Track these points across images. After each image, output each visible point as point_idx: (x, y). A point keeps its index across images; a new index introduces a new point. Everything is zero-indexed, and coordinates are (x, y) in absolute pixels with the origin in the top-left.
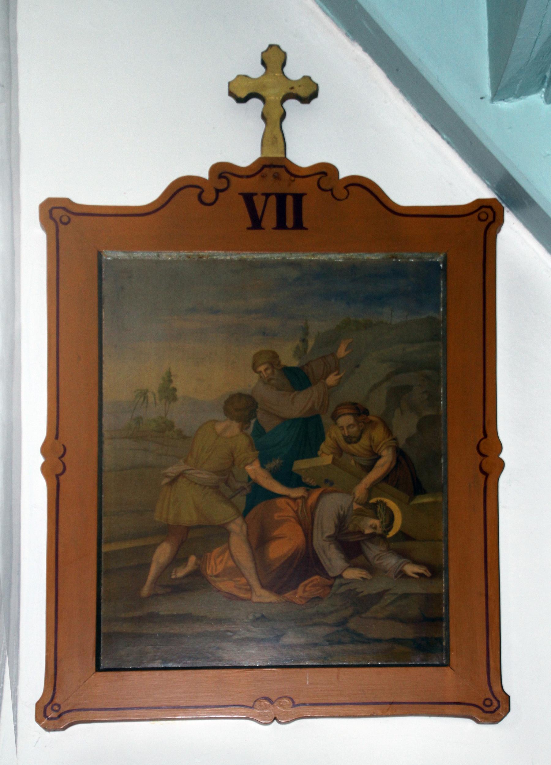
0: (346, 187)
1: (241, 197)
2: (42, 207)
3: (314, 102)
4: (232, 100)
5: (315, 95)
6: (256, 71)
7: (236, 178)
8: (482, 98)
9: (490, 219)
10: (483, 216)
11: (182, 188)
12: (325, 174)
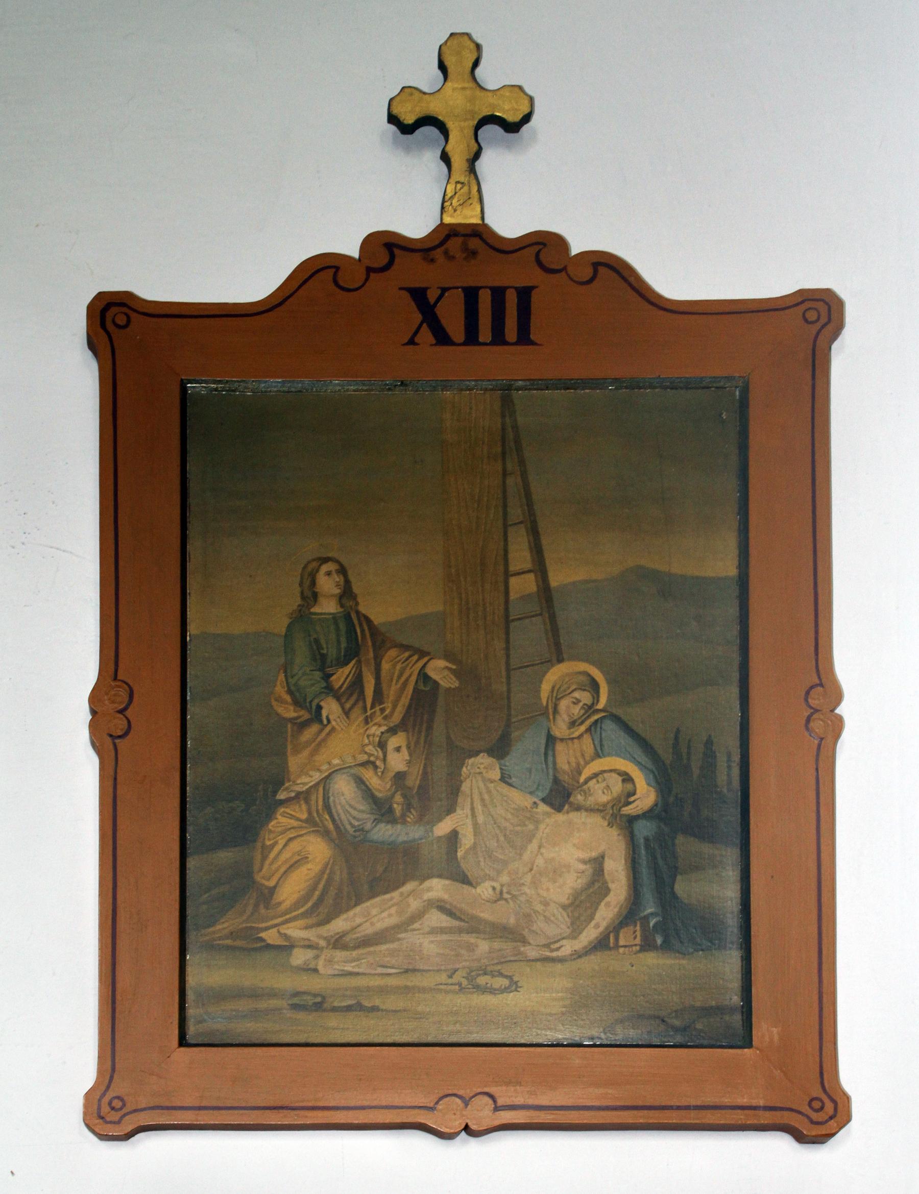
0: (596, 266)
1: (406, 294)
2: (91, 308)
3: (525, 128)
4: (393, 128)
5: (527, 118)
6: (426, 76)
7: (814, 333)
8: (12, 1173)
9: (824, 320)
10: (812, 316)
11: (319, 271)
12: (545, 245)
